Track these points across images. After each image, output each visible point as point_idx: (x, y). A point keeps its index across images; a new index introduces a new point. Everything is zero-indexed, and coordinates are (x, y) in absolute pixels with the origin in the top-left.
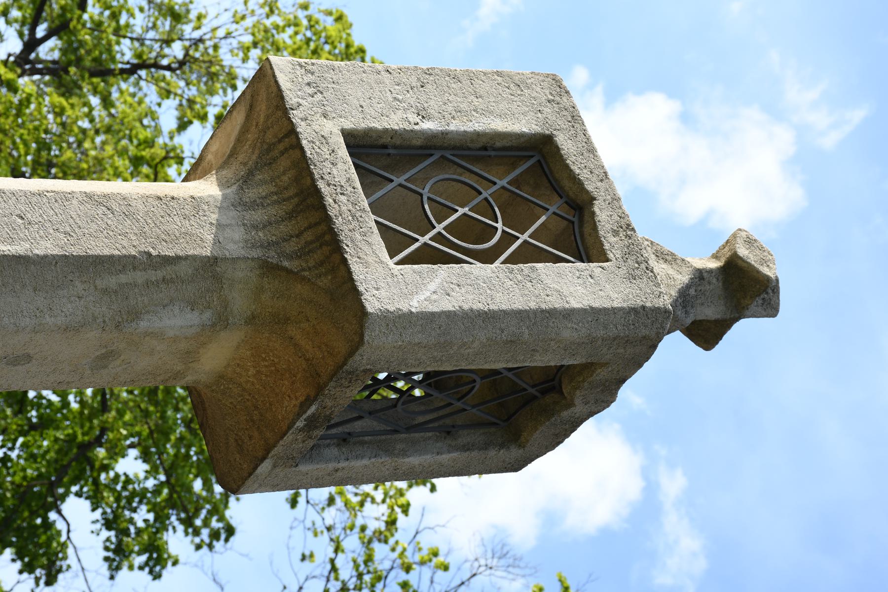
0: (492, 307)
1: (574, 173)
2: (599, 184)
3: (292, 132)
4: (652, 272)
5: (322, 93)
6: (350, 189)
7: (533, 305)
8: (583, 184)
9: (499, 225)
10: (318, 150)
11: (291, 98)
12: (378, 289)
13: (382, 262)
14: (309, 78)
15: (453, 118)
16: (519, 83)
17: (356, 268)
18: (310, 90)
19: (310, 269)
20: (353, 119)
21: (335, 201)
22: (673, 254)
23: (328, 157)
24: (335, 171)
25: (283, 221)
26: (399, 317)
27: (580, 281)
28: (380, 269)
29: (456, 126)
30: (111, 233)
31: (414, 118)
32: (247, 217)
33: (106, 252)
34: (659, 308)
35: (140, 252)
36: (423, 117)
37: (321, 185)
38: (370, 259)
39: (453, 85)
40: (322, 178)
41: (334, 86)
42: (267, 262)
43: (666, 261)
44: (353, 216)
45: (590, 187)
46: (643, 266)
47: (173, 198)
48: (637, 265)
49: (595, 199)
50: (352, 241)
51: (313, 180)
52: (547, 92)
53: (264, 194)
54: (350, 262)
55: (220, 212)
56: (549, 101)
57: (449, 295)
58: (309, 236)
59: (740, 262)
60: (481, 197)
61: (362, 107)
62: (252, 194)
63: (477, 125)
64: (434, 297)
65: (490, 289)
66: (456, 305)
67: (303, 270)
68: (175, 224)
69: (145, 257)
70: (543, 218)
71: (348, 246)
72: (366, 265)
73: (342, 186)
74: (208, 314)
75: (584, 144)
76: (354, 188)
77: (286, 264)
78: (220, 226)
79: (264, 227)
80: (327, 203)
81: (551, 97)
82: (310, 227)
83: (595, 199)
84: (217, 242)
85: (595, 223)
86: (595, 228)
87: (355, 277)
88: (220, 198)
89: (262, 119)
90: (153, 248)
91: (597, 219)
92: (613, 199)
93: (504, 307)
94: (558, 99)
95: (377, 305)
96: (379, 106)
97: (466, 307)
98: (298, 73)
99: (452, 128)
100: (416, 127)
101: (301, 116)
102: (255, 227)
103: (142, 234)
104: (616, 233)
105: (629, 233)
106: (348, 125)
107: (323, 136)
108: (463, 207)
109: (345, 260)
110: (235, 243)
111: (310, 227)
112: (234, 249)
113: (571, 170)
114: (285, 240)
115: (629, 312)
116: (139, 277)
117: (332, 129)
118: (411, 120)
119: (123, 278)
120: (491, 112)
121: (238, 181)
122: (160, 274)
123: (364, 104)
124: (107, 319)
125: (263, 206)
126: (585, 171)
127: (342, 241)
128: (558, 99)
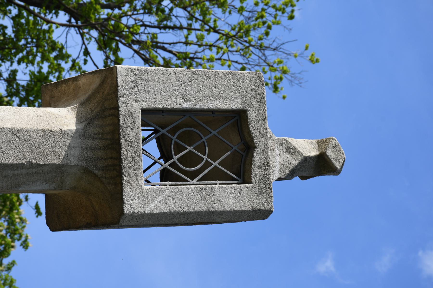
0: (185, 210)
1: (251, 132)
2: (261, 139)
3: (117, 108)
4: (271, 190)
5: (138, 87)
6: (136, 143)
7: (206, 209)
8: (253, 139)
9: (205, 157)
10: (127, 121)
11: (122, 90)
12: (133, 200)
13: (139, 185)
14: (134, 78)
15: (200, 101)
16: (239, 79)
17: (126, 189)
18: (132, 85)
19: (106, 178)
20: (149, 103)
21: (126, 150)
22: (295, 148)
23: (130, 125)
24: (131, 134)
25: (100, 149)
26: (139, 215)
27: (233, 195)
28: (137, 189)
29: (201, 105)
30: (16, 151)
31: (180, 101)
32: (85, 143)
33: (11, 162)
34: (267, 210)
35: (27, 162)
36: (185, 100)
37: (122, 141)
38: (134, 184)
39: (206, 81)
40: (124, 137)
41: (145, 83)
42: (87, 169)
43: (290, 152)
44: (133, 159)
45: (256, 141)
46: (267, 187)
47: (51, 131)
48: (264, 186)
49: (256, 148)
50: (128, 174)
51: (119, 138)
52: (252, 84)
53: (96, 132)
54: (124, 185)
55: (72, 139)
56: (252, 90)
57: (166, 203)
58: (110, 162)
59: (326, 157)
60: (202, 141)
61: (155, 95)
62: (91, 131)
63: (210, 104)
64: (159, 204)
65: (188, 200)
66: (168, 209)
67: (103, 177)
68: (48, 146)
69: (29, 164)
70: (229, 153)
71: (125, 176)
72: (131, 187)
73: (132, 142)
74: (54, 185)
75: (261, 115)
76: (138, 143)
77: (96, 171)
78: (70, 147)
79: (91, 150)
80: (122, 152)
81: (253, 87)
82: (111, 158)
83: (256, 148)
84: (66, 156)
85: (252, 161)
86: (251, 163)
87: (124, 194)
88: (74, 131)
89: (105, 93)
90: (34, 159)
91: (254, 159)
92: (266, 148)
93: (191, 210)
94: (257, 88)
95: (130, 209)
96: (165, 94)
97: (173, 210)
98: (129, 75)
99: (197, 107)
100: (180, 107)
101: (123, 101)
102: (87, 149)
103: (31, 152)
104: (260, 167)
105: (267, 167)
106: (145, 106)
107: (131, 113)
108: (190, 146)
109: (122, 184)
110: (75, 157)
111: (111, 158)
112: (73, 161)
113: (250, 131)
114: (99, 159)
115: (252, 212)
116: (24, 171)
117: (136, 108)
118: (178, 102)
119: (16, 172)
120: (220, 97)
121: (86, 120)
122: (34, 170)
123: (157, 93)
124: (4, 187)
125: (94, 138)
126: (256, 132)
127: (123, 173)
128: (257, 88)
